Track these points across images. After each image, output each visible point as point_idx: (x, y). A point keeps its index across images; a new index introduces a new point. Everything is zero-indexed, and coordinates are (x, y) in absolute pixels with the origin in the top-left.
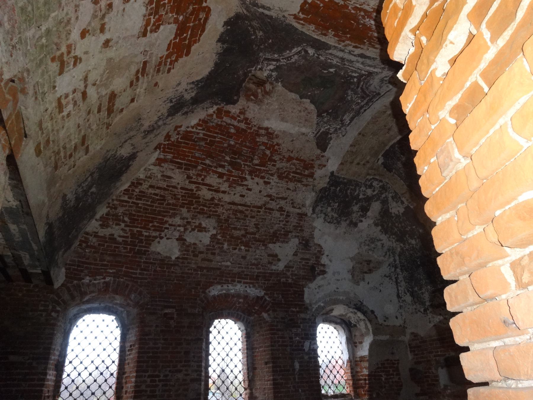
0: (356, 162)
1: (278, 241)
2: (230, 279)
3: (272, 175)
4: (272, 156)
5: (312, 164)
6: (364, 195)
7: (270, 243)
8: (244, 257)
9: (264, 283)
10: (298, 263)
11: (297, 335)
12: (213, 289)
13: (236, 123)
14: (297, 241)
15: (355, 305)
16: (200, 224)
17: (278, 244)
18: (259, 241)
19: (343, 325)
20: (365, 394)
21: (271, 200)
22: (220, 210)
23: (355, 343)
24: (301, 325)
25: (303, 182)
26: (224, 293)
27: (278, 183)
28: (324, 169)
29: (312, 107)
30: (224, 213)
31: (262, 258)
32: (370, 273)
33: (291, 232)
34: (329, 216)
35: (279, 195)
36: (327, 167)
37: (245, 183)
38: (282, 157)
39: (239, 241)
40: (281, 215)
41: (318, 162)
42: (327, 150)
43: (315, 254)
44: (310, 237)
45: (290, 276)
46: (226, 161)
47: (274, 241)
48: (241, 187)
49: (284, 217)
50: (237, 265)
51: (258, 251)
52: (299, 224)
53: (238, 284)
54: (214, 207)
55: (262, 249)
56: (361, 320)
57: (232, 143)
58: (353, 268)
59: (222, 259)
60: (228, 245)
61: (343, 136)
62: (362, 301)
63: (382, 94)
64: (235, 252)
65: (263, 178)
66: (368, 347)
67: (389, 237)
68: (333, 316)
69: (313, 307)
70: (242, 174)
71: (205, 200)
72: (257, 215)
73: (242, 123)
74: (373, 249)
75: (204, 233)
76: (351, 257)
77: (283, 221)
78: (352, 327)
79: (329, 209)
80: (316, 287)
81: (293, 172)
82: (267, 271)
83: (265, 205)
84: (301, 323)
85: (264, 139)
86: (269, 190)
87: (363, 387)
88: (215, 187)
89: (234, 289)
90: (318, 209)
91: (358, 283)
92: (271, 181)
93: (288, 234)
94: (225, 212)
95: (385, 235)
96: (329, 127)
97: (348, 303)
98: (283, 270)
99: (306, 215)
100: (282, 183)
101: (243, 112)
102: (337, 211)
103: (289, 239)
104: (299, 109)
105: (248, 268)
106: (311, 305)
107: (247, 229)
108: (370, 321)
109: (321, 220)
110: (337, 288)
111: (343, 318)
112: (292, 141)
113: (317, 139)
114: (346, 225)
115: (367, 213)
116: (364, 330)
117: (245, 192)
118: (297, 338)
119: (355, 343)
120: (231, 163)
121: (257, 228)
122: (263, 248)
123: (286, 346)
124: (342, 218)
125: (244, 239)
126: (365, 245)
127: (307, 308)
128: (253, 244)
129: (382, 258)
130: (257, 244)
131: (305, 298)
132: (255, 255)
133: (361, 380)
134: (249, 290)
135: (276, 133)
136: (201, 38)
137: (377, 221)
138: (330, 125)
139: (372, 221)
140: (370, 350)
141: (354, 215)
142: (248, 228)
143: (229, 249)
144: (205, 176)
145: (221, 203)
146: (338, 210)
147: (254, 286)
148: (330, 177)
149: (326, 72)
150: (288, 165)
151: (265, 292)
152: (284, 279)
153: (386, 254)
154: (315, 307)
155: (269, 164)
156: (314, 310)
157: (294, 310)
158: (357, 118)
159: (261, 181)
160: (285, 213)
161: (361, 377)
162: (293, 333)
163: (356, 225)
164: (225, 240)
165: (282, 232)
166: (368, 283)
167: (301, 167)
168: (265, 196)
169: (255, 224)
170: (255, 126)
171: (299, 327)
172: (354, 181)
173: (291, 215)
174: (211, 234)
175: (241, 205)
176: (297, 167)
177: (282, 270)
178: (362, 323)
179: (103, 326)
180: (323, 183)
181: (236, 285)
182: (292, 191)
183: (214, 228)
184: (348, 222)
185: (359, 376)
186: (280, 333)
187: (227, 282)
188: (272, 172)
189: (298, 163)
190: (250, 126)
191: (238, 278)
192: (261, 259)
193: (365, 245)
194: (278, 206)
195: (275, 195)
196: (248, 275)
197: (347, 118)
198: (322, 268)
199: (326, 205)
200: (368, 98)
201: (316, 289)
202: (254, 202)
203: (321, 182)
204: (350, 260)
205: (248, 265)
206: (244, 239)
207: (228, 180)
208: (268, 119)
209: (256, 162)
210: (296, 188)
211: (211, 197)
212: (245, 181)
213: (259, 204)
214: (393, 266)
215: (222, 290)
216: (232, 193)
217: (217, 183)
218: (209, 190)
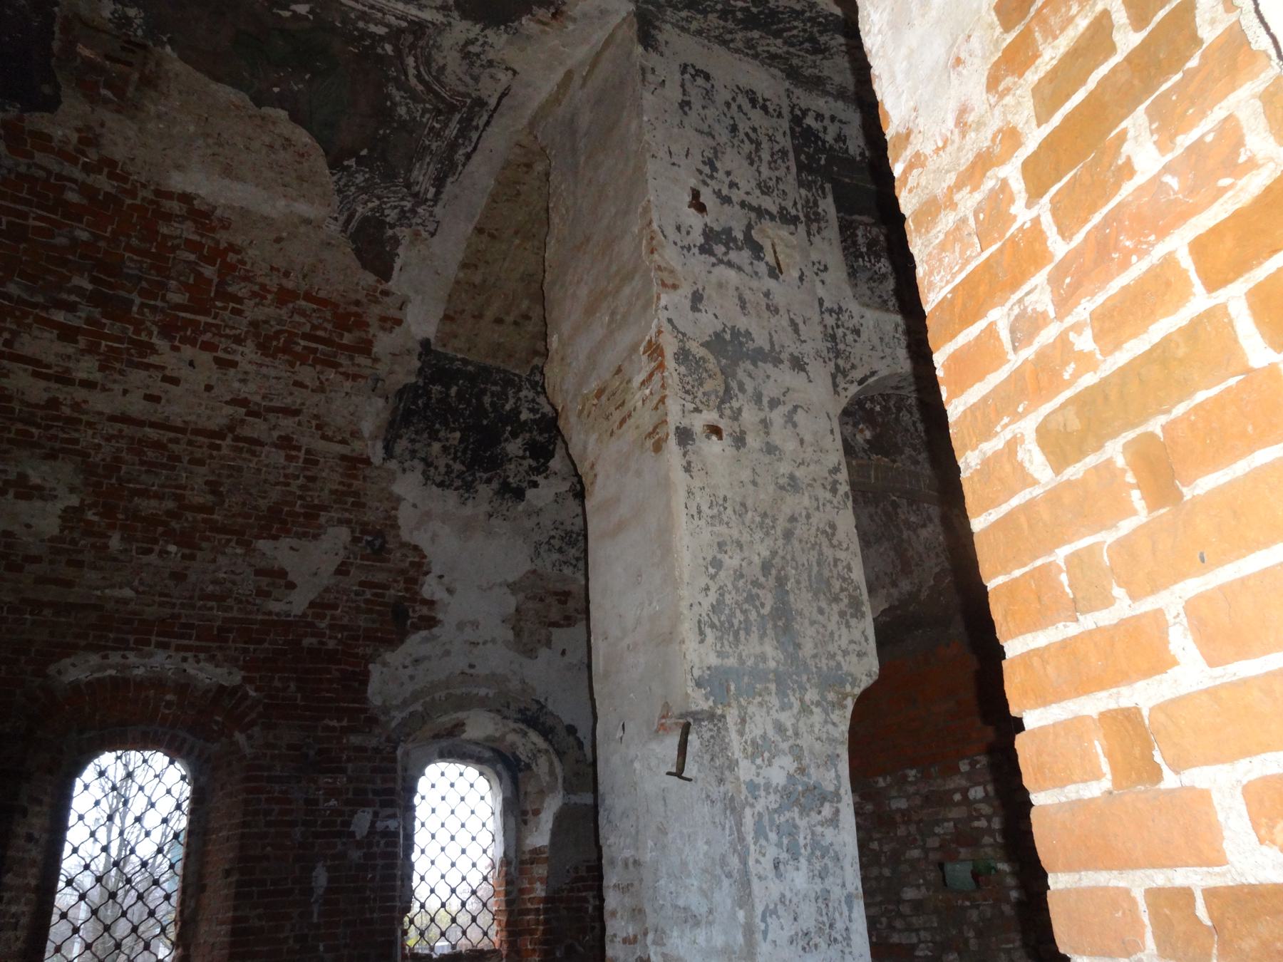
0: (490, 314)
1: (288, 532)
2: (132, 638)
3: (239, 340)
4: (222, 283)
5: (357, 315)
6: (532, 410)
7: (259, 537)
8: (179, 577)
9: (245, 651)
10: (352, 595)
11: (332, 792)
12: (74, 665)
13: (77, 174)
14: (344, 534)
15: (520, 711)
16: (23, 477)
17: (285, 542)
18: (223, 530)
19: (499, 767)
20: (534, 950)
21: (249, 414)
22: (86, 437)
23: (524, 813)
24: (350, 766)
25: (341, 365)
26: (111, 677)
27: (261, 365)
28: (397, 330)
29: (302, 137)
30: (99, 445)
31: (238, 578)
32: (569, 625)
33: (325, 508)
34: (436, 468)
35: (271, 400)
36: (404, 325)
37: (153, 359)
38: (256, 288)
39: (160, 529)
40: (290, 458)
41: (376, 310)
42: (395, 273)
43: (402, 572)
44: (386, 525)
45: (328, 632)
46: (79, 291)
47: (274, 532)
48: (144, 374)
49: (300, 464)
50: (157, 598)
51: (222, 560)
52: (350, 485)
53: (160, 651)
54: (63, 429)
55: (236, 554)
56: (539, 751)
57: (84, 236)
58: (517, 610)
59: (103, 578)
60: (122, 539)
61: (433, 234)
62: (542, 700)
63: (493, 102)
64: (145, 559)
65: (207, 347)
66: (550, 825)
68: (469, 741)
69: (394, 717)
70: (137, 332)
71: (29, 405)
72: (211, 457)
73: (100, 172)
74: (574, 562)
75: (38, 504)
76: (510, 580)
77: (297, 477)
78: (520, 770)
79: (436, 447)
80: (407, 662)
81: (305, 336)
82: (253, 617)
83: (231, 429)
84: (349, 760)
85: (187, 230)
86: (236, 385)
87: (532, 932)
88: (56, 369)
89: (144, 666)
90: (401, 446)
91: (530, 653)
92: (238, 358)
93: (319, 516)
94: (103, 443)
96: (377, 203)
97: (499, 707)
98: (304, 615)
99: (367, 462)
100: (275, 367)
101: (89, 139)
102: (459, 454)
103: (320, 527)
104: (267, 140)
105: (193, 607)
106: (386, 710)
107: (182, 497)
108: (560, 754)
109: (415, 478)
110: (472, 666)
111: (495, 745)
112: (278, 240)
113: (354, 238)
114: (491, 493)
116: (545, 779)
117: (158, 387)
118: (333, 802)
119: (524, 813)
120: (94, 299)
121: (214, 492)
122: (239, 551)
123: (292, 824)
124: (478, 475)
125: (174, 524)
126: (549, 550)
127: (372, 721)
128: (208, 539)
130: (220, 540)
131: (370, 691)
132: (214, 572)
133: (528, 912)
134: (191, 668)
135: (218, 212)
138: (379, 198)
140: (555, 833)
142: (187, 493)
143: (126, 550)
144: (15, 334)
145: (84, 418)
146: (464, 452)
147: (212, 658)
148: (420, 355)
149: (286, 14)
150: (284, 312)
151: (243, 673)
152: (314, 640)
154: (398, 716)
155: (221, 308)
156: (393, 724)
157: (334, 723)
158: (450, 180)
159: (206, 357)
160: (302, 454)
161: (529, 906)
162: (318, 789)
163: (519, 494)
164: (112, 526)
165: (297, 509)
166: (563, 653)
167: (329, 321)
168: (227, 403)
169: (206, 483)
170: (144, 186)
171: (342, 771)
172: (498, 370)
173: (322, 460)
174: (62, 507)
175: (153, 425)
176: (315, 322)
177: (300, 614)
178: (543, 760)
179: (462, 785)
180: (405, 373)
181: (151, 655)
182: (313, 391)
183: (72, 490)
184: (495, 485)
185: (524, 901)
186: (277, 787)
187: (122, 645)
188: (238, 332)
189: (314, 311)
190: (128, 186)
191: (158, 635)
192: (234, 583)
194: (275, 434)
195: (258, 399)
196: (191, 626)
197: (422, 176)
198: (425, 611)
199: (426, 435)
200: (457, 117)
201: (405, 667)
202: (193, 418)
203: (397, 368)
204: (509, 591)
205: (191, 598)
206: (174, 524)
207: (92, 349)
208: (179, 167)
210: (321, 383)
211: (45, 396)
212: (152, 353)
213: (213, 425)
215: (102, 668)
216: (118, 388)
217: (57, 355)
218: (36, 375)
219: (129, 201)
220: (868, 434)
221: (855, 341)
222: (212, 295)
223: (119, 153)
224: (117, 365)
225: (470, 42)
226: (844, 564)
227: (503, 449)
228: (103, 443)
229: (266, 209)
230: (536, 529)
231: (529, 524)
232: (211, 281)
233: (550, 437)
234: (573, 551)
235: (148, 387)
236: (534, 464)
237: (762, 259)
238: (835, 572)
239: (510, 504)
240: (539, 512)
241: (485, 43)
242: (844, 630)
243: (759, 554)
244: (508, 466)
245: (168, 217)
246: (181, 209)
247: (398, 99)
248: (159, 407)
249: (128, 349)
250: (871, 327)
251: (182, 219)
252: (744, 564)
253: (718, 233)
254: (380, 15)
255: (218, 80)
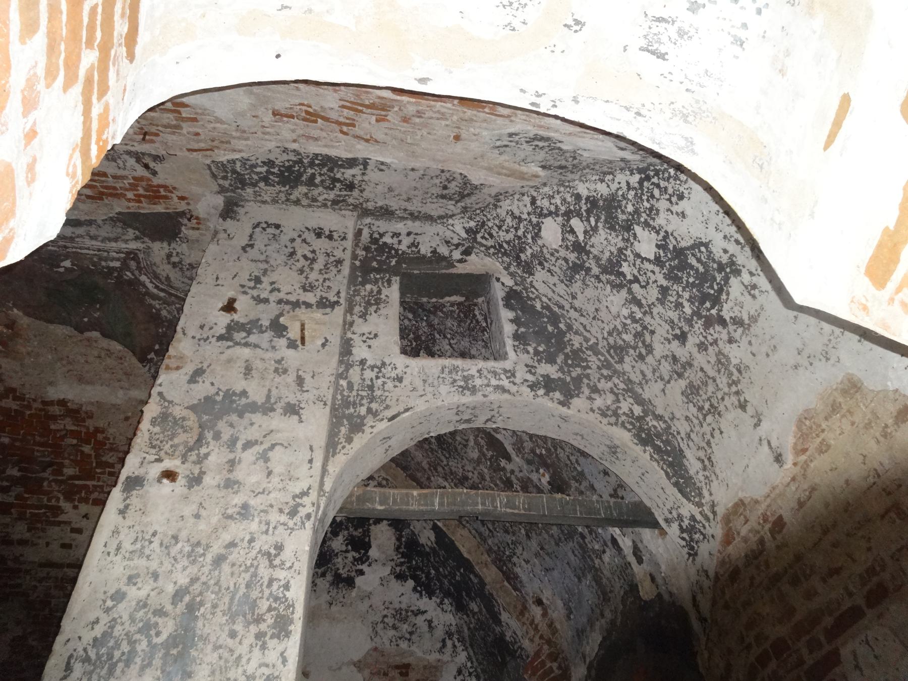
4: (97, 456)
29: (116, 346)
30: (36, 587)
37: (62, 518)
48: (57, 529)
67: (441, 603)
70: (49, 500)
73: (8, 398)
74: (408, 636)
76: (356, 659)
85: (68, 424)
94: (38, 585)
95: (430, 599)
104: (96, 353)
115: (367, 551)
126: (385, 628)
129: (437, 656)
136: (662, 472)
137: (398, 569)
139: (387, 570)
141: (339, 560)
153: (444, 645)
155: (100, 473)
163: (350, 582)
170: (34, 400)
184: (329, 577)
190: (26, 403)
193: (385, 628)
207: (21, 517)
208: (51, 384)
209: (69, 471)
214: (470, 674)
216: (42, 542)
219: (28, 412)
220: (547, 478)
221: (395, 387)
222: (94, 465)
223: (15, 383)
224: (39, 525)
225: (169, 256)
226: (282, 583)
227: (330, 546)
228: (38, 585)
229: (113, 400)
230: (370, 610)
231: (363, 607)
232: (90, 455)
233: (364, 531)
234: (405, 626)
235: (62, 538)
236: (357, 555)
237: (284, 336)
238: (267, 592)
239: (344, 592)
240: (369, 596)
241: (178, 253)
242: (257, 652)
243: (175, 583)
244: (336, 560)
245: (54, 418)
246: (60, 411)
247: (157, 306)
248: (71, 551)
249: (45, 513)
250: (415, 373)
251: (63, 416)
252: (152, 594)
253: (243, 324)
254: (105, 254)
255: (51, 322)
